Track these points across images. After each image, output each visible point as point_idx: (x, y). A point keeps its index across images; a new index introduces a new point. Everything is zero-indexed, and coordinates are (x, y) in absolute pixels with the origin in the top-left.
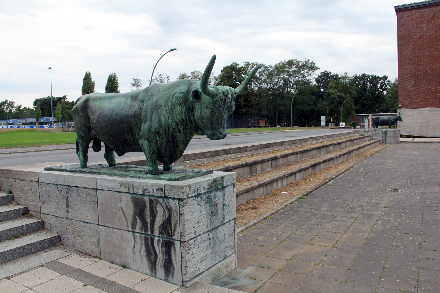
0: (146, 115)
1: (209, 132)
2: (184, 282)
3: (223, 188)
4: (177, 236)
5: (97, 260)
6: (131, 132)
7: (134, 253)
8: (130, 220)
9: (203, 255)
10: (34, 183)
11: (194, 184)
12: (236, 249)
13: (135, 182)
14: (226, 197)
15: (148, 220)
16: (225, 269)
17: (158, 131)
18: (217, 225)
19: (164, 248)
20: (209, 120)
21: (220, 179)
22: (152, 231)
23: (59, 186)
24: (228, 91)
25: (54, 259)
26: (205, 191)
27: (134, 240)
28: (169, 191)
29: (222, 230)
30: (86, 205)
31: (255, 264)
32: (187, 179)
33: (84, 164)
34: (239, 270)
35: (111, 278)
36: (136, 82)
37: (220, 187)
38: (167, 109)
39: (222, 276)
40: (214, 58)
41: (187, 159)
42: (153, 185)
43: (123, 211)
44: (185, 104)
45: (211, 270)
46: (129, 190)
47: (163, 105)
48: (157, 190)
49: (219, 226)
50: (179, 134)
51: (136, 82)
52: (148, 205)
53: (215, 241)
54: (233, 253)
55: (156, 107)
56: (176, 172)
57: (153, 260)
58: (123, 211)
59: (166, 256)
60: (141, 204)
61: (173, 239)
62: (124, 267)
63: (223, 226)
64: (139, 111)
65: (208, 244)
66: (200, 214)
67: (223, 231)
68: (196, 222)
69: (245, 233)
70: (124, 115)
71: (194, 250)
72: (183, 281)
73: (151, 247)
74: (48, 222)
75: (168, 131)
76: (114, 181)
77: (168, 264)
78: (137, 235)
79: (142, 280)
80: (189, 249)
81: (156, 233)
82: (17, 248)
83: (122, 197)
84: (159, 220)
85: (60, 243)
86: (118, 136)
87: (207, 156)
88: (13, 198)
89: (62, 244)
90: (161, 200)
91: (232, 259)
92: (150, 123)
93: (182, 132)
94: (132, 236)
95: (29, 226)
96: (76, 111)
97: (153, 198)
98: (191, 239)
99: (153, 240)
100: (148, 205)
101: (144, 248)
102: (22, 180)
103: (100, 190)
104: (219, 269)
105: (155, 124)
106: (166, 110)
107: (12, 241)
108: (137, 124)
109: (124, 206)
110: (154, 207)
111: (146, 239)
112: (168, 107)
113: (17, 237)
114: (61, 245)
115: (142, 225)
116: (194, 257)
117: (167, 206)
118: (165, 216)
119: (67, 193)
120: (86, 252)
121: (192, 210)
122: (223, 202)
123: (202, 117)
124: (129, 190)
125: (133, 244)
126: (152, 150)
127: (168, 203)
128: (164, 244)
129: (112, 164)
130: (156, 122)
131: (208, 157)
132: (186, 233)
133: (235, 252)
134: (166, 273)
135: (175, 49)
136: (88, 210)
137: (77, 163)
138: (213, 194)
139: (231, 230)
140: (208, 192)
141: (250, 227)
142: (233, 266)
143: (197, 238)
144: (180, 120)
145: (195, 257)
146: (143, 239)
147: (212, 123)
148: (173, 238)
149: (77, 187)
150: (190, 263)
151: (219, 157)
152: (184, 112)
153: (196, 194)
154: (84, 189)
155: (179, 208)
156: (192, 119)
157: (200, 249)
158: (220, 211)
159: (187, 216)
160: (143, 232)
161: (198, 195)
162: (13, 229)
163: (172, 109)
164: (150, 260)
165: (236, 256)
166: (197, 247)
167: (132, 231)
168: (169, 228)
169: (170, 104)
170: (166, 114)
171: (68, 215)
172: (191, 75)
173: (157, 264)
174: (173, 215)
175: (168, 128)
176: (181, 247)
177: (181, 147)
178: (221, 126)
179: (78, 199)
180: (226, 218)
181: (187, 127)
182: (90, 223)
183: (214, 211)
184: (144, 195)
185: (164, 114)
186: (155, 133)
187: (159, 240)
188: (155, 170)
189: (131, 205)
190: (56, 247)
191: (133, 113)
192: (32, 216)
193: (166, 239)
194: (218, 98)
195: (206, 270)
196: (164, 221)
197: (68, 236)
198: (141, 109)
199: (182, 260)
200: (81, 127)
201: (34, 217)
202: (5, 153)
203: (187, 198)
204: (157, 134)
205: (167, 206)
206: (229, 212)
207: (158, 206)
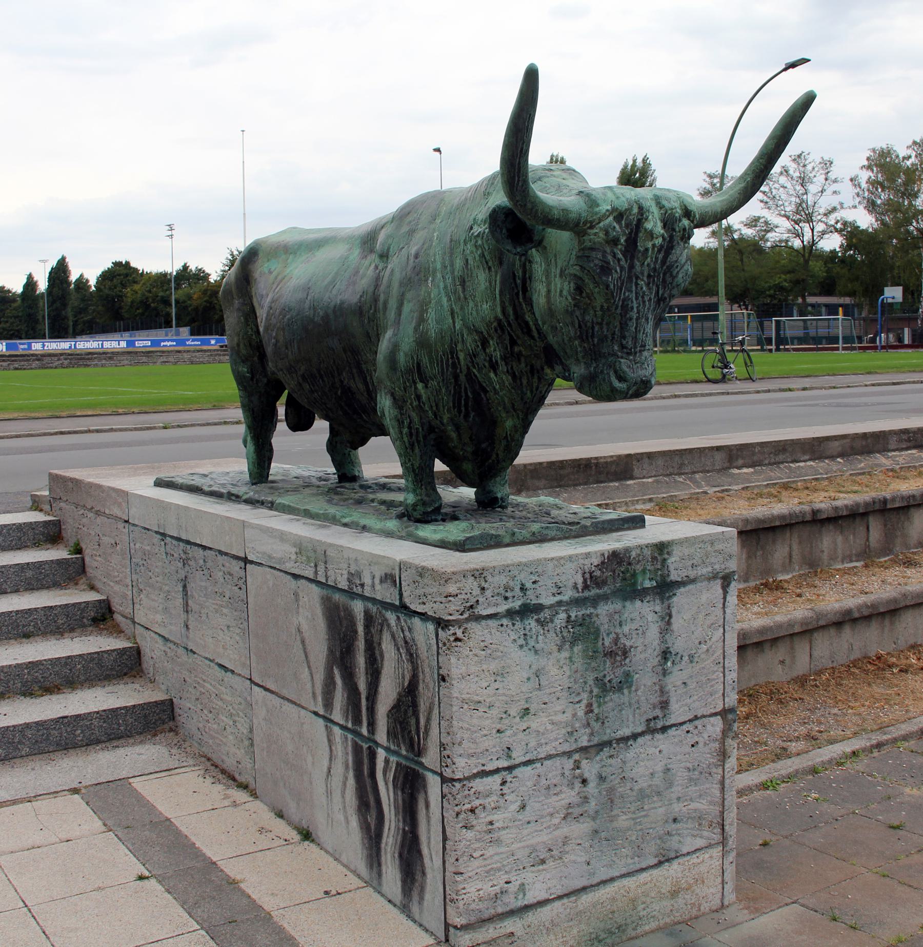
0: (385, 303)
1: (579, 370)
2: (452, 930)
3: (665, 588)
4: (431, 758)
5: (241, 796)
6: (358, 365)
7: (329, 793)
8: (320, 677)
9: (544, 837)
10: (121, 525)
11: (505, 569)
12: (731, 830)
13: (331, 545)
14: (677, 623)
15: (362, 686)
16: (667, 903)
18: (627, 732)
19: (400, 793)
20: (573, 324)
21: (648, 552)
22: (372, 725)
23: (168, 540)
24: (641, 208)
25: (124, 774)
26: (565, 598)
27: (327, 749)
28: (412, 585)
29: (652, 750)
30: (225, 611)
31: (811, 902)
32: (508, 545)
33: (260, 469)
34: (735, 913)
35: (232, 869)
36: (713, 185)
37: (647, 584)
38: (449, 281)
39: (647, 928)
40: (531, 78)
41: (740, 462)
42: (374, 560)
43: (303, 642)
44: (501, 263)
45: (586, 899)
46: (316, 573)
47: (439, 266)
48: (381, 582)
49: (635, 736)
50: (492, 375)
51: (713, 185)
52: (360, 629)
53: (611, 790)
54: (710, 846)
55: (419, 273)
57: (373, 827)
58: (303, 642)
59: (404, 821)
60: (345, 623)
61: (422, 764)
62: (307, 835)
63: (658, 736)
64: (371, 289)
65: (576, 800)
66: (534, 683)
67: (647, 759)
68: (513, 711)
69: (861, 765)
70: (333, 304)
71: (499, 818)
72: (447, 925)
73: (368, 781)
74: (147, 650)
75: (454, 364)
76: (282, 537)
77: (409, 852)
78: (337, 730)
79: (326, 893)
80: (472, 811)
81: (381, 736)
82: (27, 726)
83: (301, 595)
84: (388, 692)
85: (171, 723)
86: (321, 377)
87: (828, 453)
88: (82, 569)
89: (174, 730)
90: (391, 617)
91: (703, 868)
92: (395, 335)
93: (502, 367)
94: (325, 734)
95: (92, 659)
96: (228, 292)
97: (374, 609)
98: (484, 774)
99: (373, 756)
100: (360, 629)
101: (351, 781)
102: (98, 513)
104: (633, 901)
105: (407, 342)
106: (445, 287)
107: (33, 700)
108: (368, 335)
109: (305, 627)
110: (376, 639)
111: (357, 749)
112: (453, 273)
113: (50, 689)
114: (171, 730)
115: (348, 698)
116: (498, 842)
117: (406, 642)
118: (403, 678)
119: (184, 564)
120: (224, 766)
121: (493, 666)
122: (663, 641)
123: (551, 312)
124: (316, 573)
125: (326, 763)
126: (405, 430)
127: (410, 629)
128: (401, 779)
129: (347, 474)
130: (410, 331)
131: (832, 457)
132: (458, 750)
133: (723, 842)
134: (404, 882)
135: (805, 61)
136: (228, 627)
137: (235, 466)
138: (604, 610)
139: (706, 755)
140: (577, 602)
141: (895, 740)
142: (710, 894)
143: (516, 772)
144: (489, 324)
145: (509, 841)
146: (350, 748)
147: (585, 333)
148: (423, 760)
149: (204, 548)
150: (476, 863)
151: (881, 459)
152: (497, 292)
153: (517, 604)
155: (438, 654)
156: (528, 318)
157: (528, 815)
158: (645, 680)
159: (459, 689)
160: (350, 725)
161: (526, 611)
162: (40, 663)
163: (463, 282)
164: (365, 826)
165: (731, 857)
166: (515, 807)
167: (324, 717)
168: (413, 721)
169: (459, 263)
170: (445, 300)
171: (187, 637)
172: (910, 152)
173: (383, 845)
174: (421, 676)
175: (453, 352)
176: (443, 797)
177: (509, 424)
178: (623, 347)
179: (206, 588)
180: (674, 706)
181: (516, 349)
182: (233, 672)
183: (613, 674)
184: (351, 594)
185: (439, 302)
186: (409, 371)
187: (387, 761)
188: (424, 504)
189: (321, 624)
190: (155, 735)
191: (354, 299)
192: (117, 631)
193: (404, 762)
194: (597, 235)
195: (560, 897)
196: (399, 694)
197: (189, 705)
198: (377, 280)
199: (444, 848)
200: (238, 345)
201: (122, 632)
202: (225, 423)
203: (467, 620)
205: (406, 642)
206: (692, 685)
207: (384, 637)
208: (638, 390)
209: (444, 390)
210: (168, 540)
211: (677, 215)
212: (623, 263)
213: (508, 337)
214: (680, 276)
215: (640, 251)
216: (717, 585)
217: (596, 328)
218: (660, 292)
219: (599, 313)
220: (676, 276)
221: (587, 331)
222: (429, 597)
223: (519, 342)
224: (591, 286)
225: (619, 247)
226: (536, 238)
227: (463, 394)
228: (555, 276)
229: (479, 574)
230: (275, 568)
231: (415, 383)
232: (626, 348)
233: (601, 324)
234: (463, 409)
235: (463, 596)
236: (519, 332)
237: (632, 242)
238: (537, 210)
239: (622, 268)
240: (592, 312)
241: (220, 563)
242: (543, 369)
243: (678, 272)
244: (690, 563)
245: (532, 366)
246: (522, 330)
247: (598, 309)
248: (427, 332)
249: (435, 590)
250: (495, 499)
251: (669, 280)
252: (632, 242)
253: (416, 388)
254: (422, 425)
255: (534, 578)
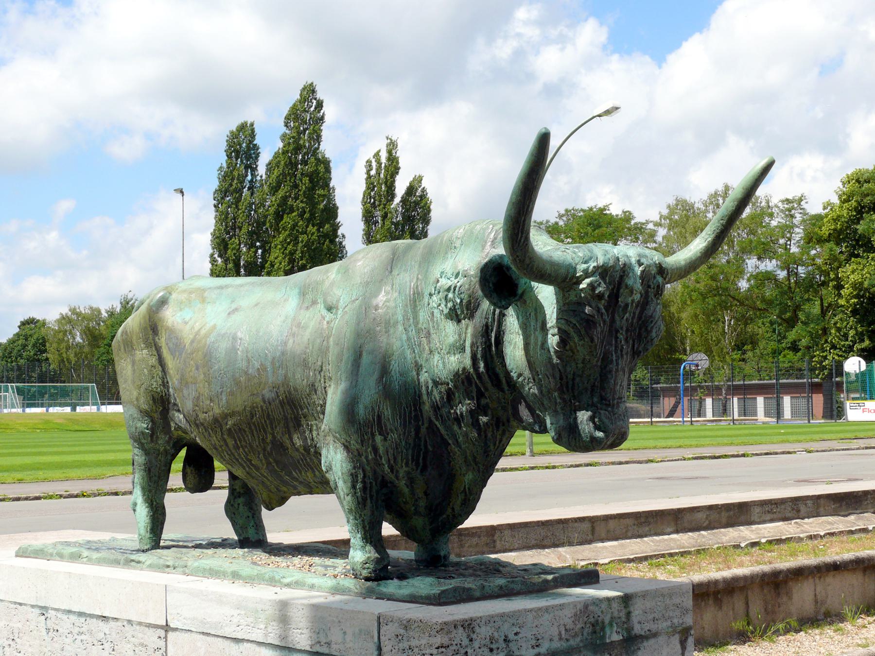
11: (490, 620)
17: (379, 417)
20: (554, 377)
37: (616, 637)
47: (400, 318)
56: (460, 570)
76: (220, 600)
103: (176, 629)
154: (128, 627)
156: (499, 370)
177: (469, 476)
204: (376, 429)
208: (614, 441)
209: (403, 443)
210: (52, 613)
211: (653, 272)
212: (605, 317)
213: (474, 390)
214: (654, 331)
215: (620, 306)
216: (676, 640)
217: (578, 379)
218: (636, 346)
219: (580, 365)
220: (651, 331)
221: (567, 383)
222: (416, 650)
223: (487, 394)
224: (576, 340)
225: (603, 301)
226: (520, 291)
227: (422, 447)
228: (535, 330)
229: (468, 625)
230: (208, 634)
231: (373, 435)
232: (605, 400)
233: (581, 376)
234: (421, 461)
235: (454, 647)
236: (489, 385)
237: (614, 296)
238: (533, 266)
239: (604, 321)
240: (573, 364)
241: (129, 636)
242: (508, 421)
243: (652, 328)
244: (651, 617)
245: (498, 419)
246: (492, 382)
247: (580, 362)
248: (390, 384)
249: (423, 642)
250: (439, 557)
251: (644, 334)
252: (614, 296)
253: (374, 440)
254: (376, 479)
255: (516, 629)
